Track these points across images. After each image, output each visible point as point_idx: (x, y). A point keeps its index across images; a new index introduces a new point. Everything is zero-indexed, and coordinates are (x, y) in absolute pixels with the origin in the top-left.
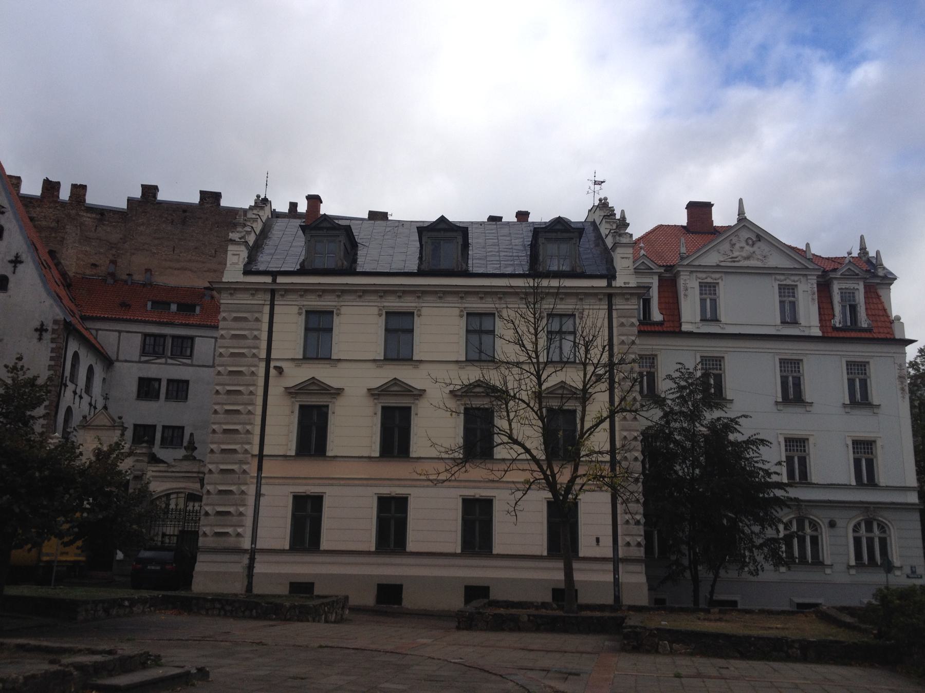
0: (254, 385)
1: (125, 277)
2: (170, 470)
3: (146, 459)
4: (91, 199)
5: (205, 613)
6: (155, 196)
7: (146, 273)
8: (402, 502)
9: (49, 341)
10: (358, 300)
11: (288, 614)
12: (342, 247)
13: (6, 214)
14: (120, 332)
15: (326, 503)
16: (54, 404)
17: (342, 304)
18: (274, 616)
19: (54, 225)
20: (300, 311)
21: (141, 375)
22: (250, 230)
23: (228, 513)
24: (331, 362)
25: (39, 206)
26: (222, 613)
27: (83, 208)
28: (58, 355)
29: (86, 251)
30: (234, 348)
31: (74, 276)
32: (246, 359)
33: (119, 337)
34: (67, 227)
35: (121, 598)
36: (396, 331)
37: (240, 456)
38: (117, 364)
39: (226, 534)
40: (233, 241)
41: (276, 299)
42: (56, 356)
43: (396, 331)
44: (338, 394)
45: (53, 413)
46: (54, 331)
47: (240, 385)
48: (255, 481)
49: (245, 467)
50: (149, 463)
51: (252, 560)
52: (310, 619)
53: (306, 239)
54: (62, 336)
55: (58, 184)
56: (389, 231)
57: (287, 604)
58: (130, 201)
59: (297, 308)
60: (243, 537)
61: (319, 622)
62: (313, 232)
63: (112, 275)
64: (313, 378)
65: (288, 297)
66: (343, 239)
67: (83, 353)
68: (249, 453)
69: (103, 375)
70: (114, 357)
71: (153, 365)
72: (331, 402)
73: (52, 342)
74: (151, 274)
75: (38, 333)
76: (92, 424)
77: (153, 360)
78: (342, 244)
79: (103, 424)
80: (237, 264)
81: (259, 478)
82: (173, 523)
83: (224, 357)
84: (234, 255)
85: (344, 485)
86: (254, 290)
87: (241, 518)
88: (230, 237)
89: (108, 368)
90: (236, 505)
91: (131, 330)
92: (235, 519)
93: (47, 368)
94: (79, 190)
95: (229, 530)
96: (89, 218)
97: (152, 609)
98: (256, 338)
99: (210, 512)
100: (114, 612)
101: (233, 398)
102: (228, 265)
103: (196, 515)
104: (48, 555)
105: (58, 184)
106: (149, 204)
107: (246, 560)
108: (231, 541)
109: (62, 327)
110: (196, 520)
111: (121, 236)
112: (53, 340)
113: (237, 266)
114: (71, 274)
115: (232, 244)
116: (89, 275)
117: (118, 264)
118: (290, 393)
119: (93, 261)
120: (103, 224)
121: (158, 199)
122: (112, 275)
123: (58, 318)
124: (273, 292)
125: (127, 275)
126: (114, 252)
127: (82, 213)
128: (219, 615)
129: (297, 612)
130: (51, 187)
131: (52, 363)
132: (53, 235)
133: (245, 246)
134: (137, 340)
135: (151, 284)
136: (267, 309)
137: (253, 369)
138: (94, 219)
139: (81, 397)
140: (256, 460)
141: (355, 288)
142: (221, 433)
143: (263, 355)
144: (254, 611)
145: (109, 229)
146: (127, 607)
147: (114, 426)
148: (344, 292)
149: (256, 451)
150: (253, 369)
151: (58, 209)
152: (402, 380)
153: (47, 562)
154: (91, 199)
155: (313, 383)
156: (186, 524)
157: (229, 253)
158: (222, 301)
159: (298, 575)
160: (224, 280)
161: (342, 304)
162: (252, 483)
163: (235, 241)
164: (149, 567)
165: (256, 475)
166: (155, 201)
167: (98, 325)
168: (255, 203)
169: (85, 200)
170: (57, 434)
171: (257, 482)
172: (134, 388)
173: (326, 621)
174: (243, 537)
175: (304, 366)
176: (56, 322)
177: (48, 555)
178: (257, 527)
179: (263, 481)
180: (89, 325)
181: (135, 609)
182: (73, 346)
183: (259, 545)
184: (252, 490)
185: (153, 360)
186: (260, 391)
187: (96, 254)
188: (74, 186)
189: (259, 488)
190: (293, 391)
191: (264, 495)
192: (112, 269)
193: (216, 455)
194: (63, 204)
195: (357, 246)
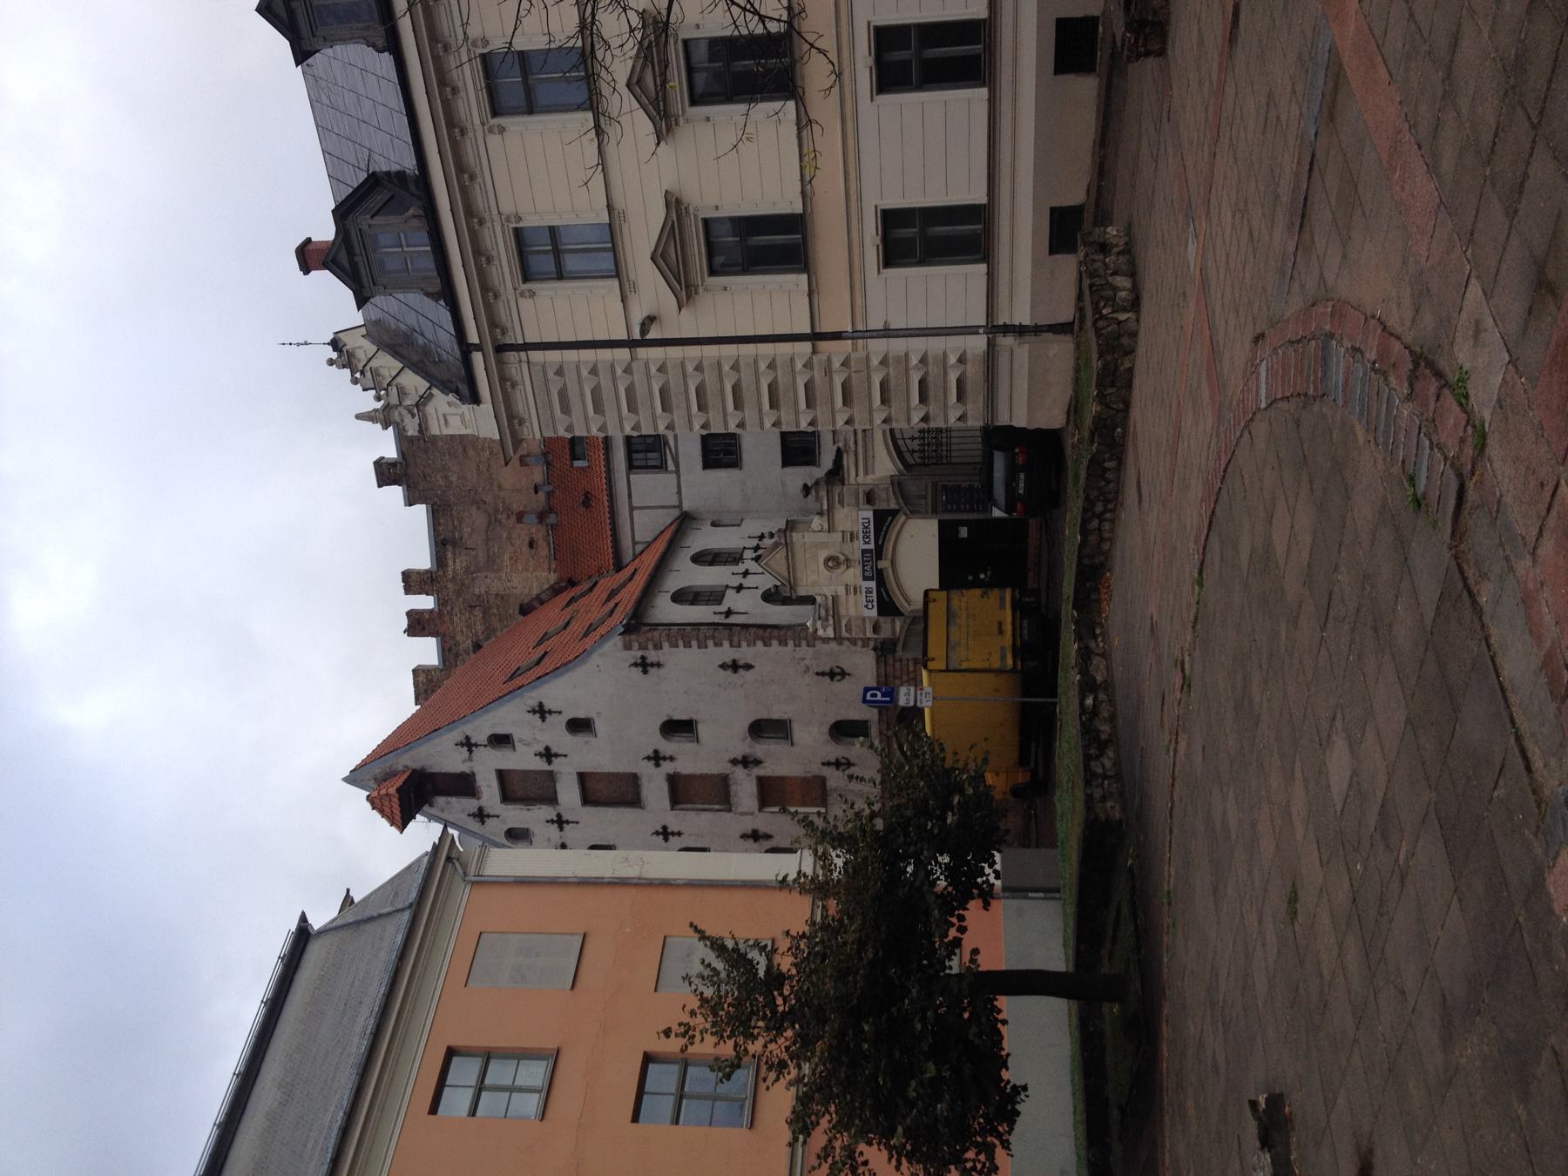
1: (542, 495)
2: (853, 447)
3: (837, 489)
4: (422, 560)
5: (1108, 543)
6: (392, 464)
12: (379, 220)
13: (467, 733)
14: (632, 509)
16: (760, 632)
17: (495, 212)
18: (1119, 430)
19: (478, 612)
20: (527, 294)
22: (395, 389)
23: (922, 382)
24: (617, 223)
27: (441, 573)
28: (680, 637)
31: (555, 571)
35: (1080, 715)
37: (818, 375)
38: (686, 507)
39: (960, 383)
40: (422, 428)
41: (513, 342)
44: (678, 202)
45: (775, 632)
46: (641, 648)
47: (686, 391)
50: (843, 483)
51: (1007, 329)
52: (1128, 365)
53: (381, 294)
54: (649, 635)
55: (410, 614)
56: (329, 98)
57: (1095, 408)
58: (410, 502)
62: (366, 284)
63: (541, 517)
64: (653, 258)
66: (364, 221)
68: (811, 358)
69: (707, 528)
70: (676, 513)
72: (695, 215)
73: (661, 648)
74: (527, 456)
75: (649, 668)
79: (784, 562)
80: (462, 416)
81: (856, 335)
82: (944, 440)
83: (639, 422)
84: (446, 422)
85: (859, 178)
86: (505, 384)
88: (416, 434)
92: (933, 370)
93: (704, 650)
94: (413, 582)
95: (953, 378)
96: (454, 562)
97: (1098, 631)
98: (594, 371)
99: (922, 414)
100: (1105, 728)
101: (712, 399)
103: (929, 445)
104: (1003, 657)
105: (410, 614)
107: (1006, 341)
108: (974, 372)
109: (633, 637)
110: (937, 445)
111: (474, 508)
112: (658, 647)
114: (553, 577)
115: (427, 429)
118: (689, 297)
119: (525, 548)
124: (500, 349)
125: (536, 492)
127: (450, 574)
128: (1112, 521)
130: (417, 624)
131: (694, 643)
132: (495, 610)
133: (425, 405)
134: (641, 480)
135: (545, 454)
136: (536, 356)
137: (653, 370)
138: (454, 554)
139: (729, 613)
140: (824, 346)
142: (779, 410)
143: (623, 354)
144: (1107, 464)
148: (470, 212)
149: (806, 347)
150: (653, 370)
152: (629, 73)
153: (1015, 657)
154: (422, 560)
156: (945, 461)
159: (1035, 232)
160: (498, 438)
161: (495, 212)
162: (865, 347)
163: (420, 425)
164: (1021, 492)
165: (850, 342)
166: (401, 463)
167: (626, 542)
168: (344, 367)
169: (427, 571)
171: (863, 338)
172: (722, 476)
173: (1135, 304)
175: (632, 277)
176: (628, 647)
177: (1003, 657)
179: (860, 327)
181: (1099, 679)
183: (980, 319)
184: (878, 347)
188: (409, 590)
189: (874, 334)
191: (886, 322)
192: (532, 519)
193: (819, 415)
194: (440, 602)
195: (374, 173)
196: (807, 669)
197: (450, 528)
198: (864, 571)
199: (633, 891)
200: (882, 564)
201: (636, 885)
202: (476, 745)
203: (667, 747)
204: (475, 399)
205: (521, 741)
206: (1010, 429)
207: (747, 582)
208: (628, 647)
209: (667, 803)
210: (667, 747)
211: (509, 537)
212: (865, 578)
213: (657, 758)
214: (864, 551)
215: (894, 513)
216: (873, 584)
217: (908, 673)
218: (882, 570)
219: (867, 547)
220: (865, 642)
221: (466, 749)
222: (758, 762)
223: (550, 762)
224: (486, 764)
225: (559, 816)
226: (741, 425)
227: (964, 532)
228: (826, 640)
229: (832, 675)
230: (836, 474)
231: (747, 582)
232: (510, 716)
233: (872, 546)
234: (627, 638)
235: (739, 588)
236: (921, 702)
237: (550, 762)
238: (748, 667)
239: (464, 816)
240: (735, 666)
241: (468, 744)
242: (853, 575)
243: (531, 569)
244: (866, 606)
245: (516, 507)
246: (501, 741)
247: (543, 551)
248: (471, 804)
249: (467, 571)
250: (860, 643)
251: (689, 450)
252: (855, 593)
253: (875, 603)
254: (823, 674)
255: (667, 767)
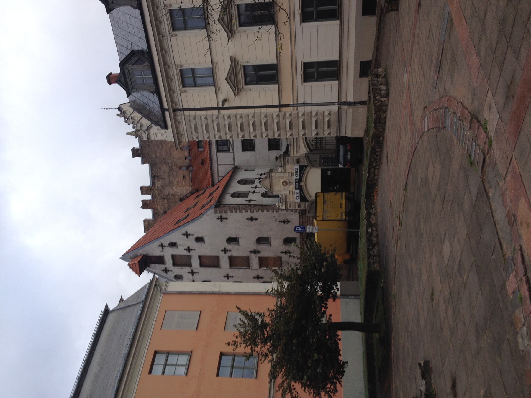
0: (236, 116)
1: (187, 161)
3: (287, 158)
4: (147, 183)
6: (138, 150)
7: (183, 150)
8: (306, 66)
9: (227, 214)
10: (168, 53)
11: (380, 130)
12: (134, 66)
14: (218, 165)
15: (308, 60)
16: (260, 207)
17: (173, 63)
18: (381, 138)
19: (166, 201)
21: (241, 150)
22: (139, 124)
23: (316, 122)
25: (157, 209)
26: (377, 167)
29: (177, 182)
30: (214, 131)
31: (192, 187)
32: (220, 122)
33: (221, 165)
34: (165, 194)
36: (185, 21)
38: (236, 164)
39: (329, 122)
40: (148, 138)
42: (234, 209)
43: (185, 21)
44: (235, 60)
45: (265, 207)
46: (221, 212)
48: (296, 108)
49: (287, 115)
50: (289, 156)
51: (345, 103)
52: (384, 116)
56: (118, 24)
58: (143, 163)
59: (182, 94)
60: (331, 111)
61: (387, 105)
62: (130, 88)
64: (226, 79)
65: (176, 100)
66: (130, 67)
67: (232, 190)
68: (279, 113)
71: (234, 144)
73: (227, 213)
74: (183, 147)
76: (270, 188)
77: (231, 145)
78: (132, 67)
79: (269, 183)
80: (162, 134)
81: (294, 105)
82: (323, 141)
86: (176, 123)
87: (319, 114)
88: (146, 140)
89: (239, 168)
90: (311, 117)
91: (216, 160)
94: (144, 190)
96: (158, 183)
98: (206, 118)
99: (316, 133)
100: (375, 239)
102: (163, 139)
104: (342, 216)
105: (143, 201)
106: (143, 152)
107: (345, 107)
108: (334, 118)
109: (218, 209)
111: (165, 165)
113: (163, 134)
114: (191, 189)
115: (150, 138)
116: (190, 179)
117: (181, 165)
118: (238, 93)
119: (182, 178)
120: (160, 175)
121: (139, 147)
122: (187, 168)
123: (213, 212)
124: (175, 110)
125: (186, 159)
126: (174, 168)
127: (156, 187)
128: (378, 169)
129: (378, 125)
130: (145, 205)
131: (238, 211)
134: (220, 155)
135: (189, 146)
136: (187, 113)
137: (226, 118)
138: (158, 180)
139: (250, 201)
140: (283, 109)
141: (161, 57)
143: (216, 112)
144: (377, 150)
145: (162, 172)
146: (372, 230)
147: (270, 177)
149: (277, 109)
150: (226, 118)
151: (157, 200)
154: (147, 183)
155: (229, 78)
157: (156, 139)
158: (187, 140)
160: (173, 141)
161: (173, 63)
162: (297, 109)
163: (148, 136)
164: (349, 159)
165: (292, 108)
167: (216, 176)
168: (122, 117)
169: (149, 187)
170: (277, 204)
171: (296, 106)
172: (248, 154)
173: (387, 95)
174: (331, 111)
176: (216, 212)
177: (342, 216)
178: (324, 103)
179: (296, 103)
180: (216, 181)
182: (229, 200)
183: (336, 100)
184: (301, 109)
185: (231, 145)
186: (239, 111)
187: (177, 177)
188: (142, 193)
190: (236, 91)
191: (304, 101)
192: (184, 168)
194: (153, 197)
195: (133, 50)
196: (276, 220)
197: (157, 172)
198: (296, 186)
199: (217, 296)
200: (302, 184)
201: (218, 294)
202: (165, 246)
203: (229, 247)
204: (166, 127)
205: (180, 245)
206: (345, 137)
207: (256, 190)
208: (216, 212)
209: (228, 266)
210: (229, 247)
211: (176, 175)
212: (296, 189)
213: (225, 251)
214: (296, 179)
215: (306, 166)
216: (298, 191)
217: (310, 221)
218: (301, 186)
219: (297, 178)
220: (296, 211)
221: (161, 247)
222: (259, 252)
223: (189, 252)
224: (168, 253)
225: (192, 271)
226: (255, 136)
227: (329, 173)
228: (282, 210)
229: (284, 222)
230: (287, 153)
231: (256, 190)
232: (176, 236)
233: (298, 178)
234: (216, 209)
235: (254, 192)
236: (314, 231)
237: (189, 252)
238: (256, 219)
239: (160, 271)
240: (252, 219)
241: (162, 246)
242: (292, 188)
243: (183, 186)
244: (296, 198)
245: (179, 164)
246: (173, 245)
247: (188, 179)
248: (163, 267)
249: (162, 186)
250: (294, 211)
251: (237, 144)
252: (292, 194)
253: (299, 197)
254: (281, 222)
255: (229, 254)
